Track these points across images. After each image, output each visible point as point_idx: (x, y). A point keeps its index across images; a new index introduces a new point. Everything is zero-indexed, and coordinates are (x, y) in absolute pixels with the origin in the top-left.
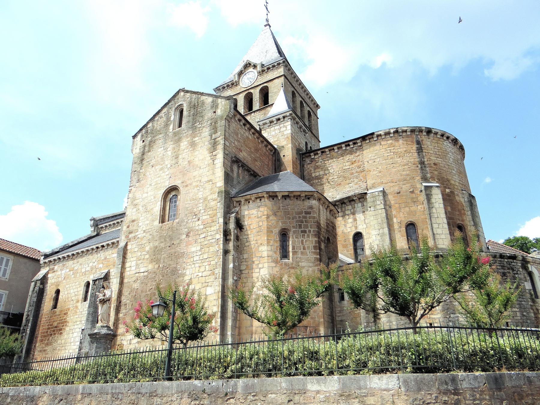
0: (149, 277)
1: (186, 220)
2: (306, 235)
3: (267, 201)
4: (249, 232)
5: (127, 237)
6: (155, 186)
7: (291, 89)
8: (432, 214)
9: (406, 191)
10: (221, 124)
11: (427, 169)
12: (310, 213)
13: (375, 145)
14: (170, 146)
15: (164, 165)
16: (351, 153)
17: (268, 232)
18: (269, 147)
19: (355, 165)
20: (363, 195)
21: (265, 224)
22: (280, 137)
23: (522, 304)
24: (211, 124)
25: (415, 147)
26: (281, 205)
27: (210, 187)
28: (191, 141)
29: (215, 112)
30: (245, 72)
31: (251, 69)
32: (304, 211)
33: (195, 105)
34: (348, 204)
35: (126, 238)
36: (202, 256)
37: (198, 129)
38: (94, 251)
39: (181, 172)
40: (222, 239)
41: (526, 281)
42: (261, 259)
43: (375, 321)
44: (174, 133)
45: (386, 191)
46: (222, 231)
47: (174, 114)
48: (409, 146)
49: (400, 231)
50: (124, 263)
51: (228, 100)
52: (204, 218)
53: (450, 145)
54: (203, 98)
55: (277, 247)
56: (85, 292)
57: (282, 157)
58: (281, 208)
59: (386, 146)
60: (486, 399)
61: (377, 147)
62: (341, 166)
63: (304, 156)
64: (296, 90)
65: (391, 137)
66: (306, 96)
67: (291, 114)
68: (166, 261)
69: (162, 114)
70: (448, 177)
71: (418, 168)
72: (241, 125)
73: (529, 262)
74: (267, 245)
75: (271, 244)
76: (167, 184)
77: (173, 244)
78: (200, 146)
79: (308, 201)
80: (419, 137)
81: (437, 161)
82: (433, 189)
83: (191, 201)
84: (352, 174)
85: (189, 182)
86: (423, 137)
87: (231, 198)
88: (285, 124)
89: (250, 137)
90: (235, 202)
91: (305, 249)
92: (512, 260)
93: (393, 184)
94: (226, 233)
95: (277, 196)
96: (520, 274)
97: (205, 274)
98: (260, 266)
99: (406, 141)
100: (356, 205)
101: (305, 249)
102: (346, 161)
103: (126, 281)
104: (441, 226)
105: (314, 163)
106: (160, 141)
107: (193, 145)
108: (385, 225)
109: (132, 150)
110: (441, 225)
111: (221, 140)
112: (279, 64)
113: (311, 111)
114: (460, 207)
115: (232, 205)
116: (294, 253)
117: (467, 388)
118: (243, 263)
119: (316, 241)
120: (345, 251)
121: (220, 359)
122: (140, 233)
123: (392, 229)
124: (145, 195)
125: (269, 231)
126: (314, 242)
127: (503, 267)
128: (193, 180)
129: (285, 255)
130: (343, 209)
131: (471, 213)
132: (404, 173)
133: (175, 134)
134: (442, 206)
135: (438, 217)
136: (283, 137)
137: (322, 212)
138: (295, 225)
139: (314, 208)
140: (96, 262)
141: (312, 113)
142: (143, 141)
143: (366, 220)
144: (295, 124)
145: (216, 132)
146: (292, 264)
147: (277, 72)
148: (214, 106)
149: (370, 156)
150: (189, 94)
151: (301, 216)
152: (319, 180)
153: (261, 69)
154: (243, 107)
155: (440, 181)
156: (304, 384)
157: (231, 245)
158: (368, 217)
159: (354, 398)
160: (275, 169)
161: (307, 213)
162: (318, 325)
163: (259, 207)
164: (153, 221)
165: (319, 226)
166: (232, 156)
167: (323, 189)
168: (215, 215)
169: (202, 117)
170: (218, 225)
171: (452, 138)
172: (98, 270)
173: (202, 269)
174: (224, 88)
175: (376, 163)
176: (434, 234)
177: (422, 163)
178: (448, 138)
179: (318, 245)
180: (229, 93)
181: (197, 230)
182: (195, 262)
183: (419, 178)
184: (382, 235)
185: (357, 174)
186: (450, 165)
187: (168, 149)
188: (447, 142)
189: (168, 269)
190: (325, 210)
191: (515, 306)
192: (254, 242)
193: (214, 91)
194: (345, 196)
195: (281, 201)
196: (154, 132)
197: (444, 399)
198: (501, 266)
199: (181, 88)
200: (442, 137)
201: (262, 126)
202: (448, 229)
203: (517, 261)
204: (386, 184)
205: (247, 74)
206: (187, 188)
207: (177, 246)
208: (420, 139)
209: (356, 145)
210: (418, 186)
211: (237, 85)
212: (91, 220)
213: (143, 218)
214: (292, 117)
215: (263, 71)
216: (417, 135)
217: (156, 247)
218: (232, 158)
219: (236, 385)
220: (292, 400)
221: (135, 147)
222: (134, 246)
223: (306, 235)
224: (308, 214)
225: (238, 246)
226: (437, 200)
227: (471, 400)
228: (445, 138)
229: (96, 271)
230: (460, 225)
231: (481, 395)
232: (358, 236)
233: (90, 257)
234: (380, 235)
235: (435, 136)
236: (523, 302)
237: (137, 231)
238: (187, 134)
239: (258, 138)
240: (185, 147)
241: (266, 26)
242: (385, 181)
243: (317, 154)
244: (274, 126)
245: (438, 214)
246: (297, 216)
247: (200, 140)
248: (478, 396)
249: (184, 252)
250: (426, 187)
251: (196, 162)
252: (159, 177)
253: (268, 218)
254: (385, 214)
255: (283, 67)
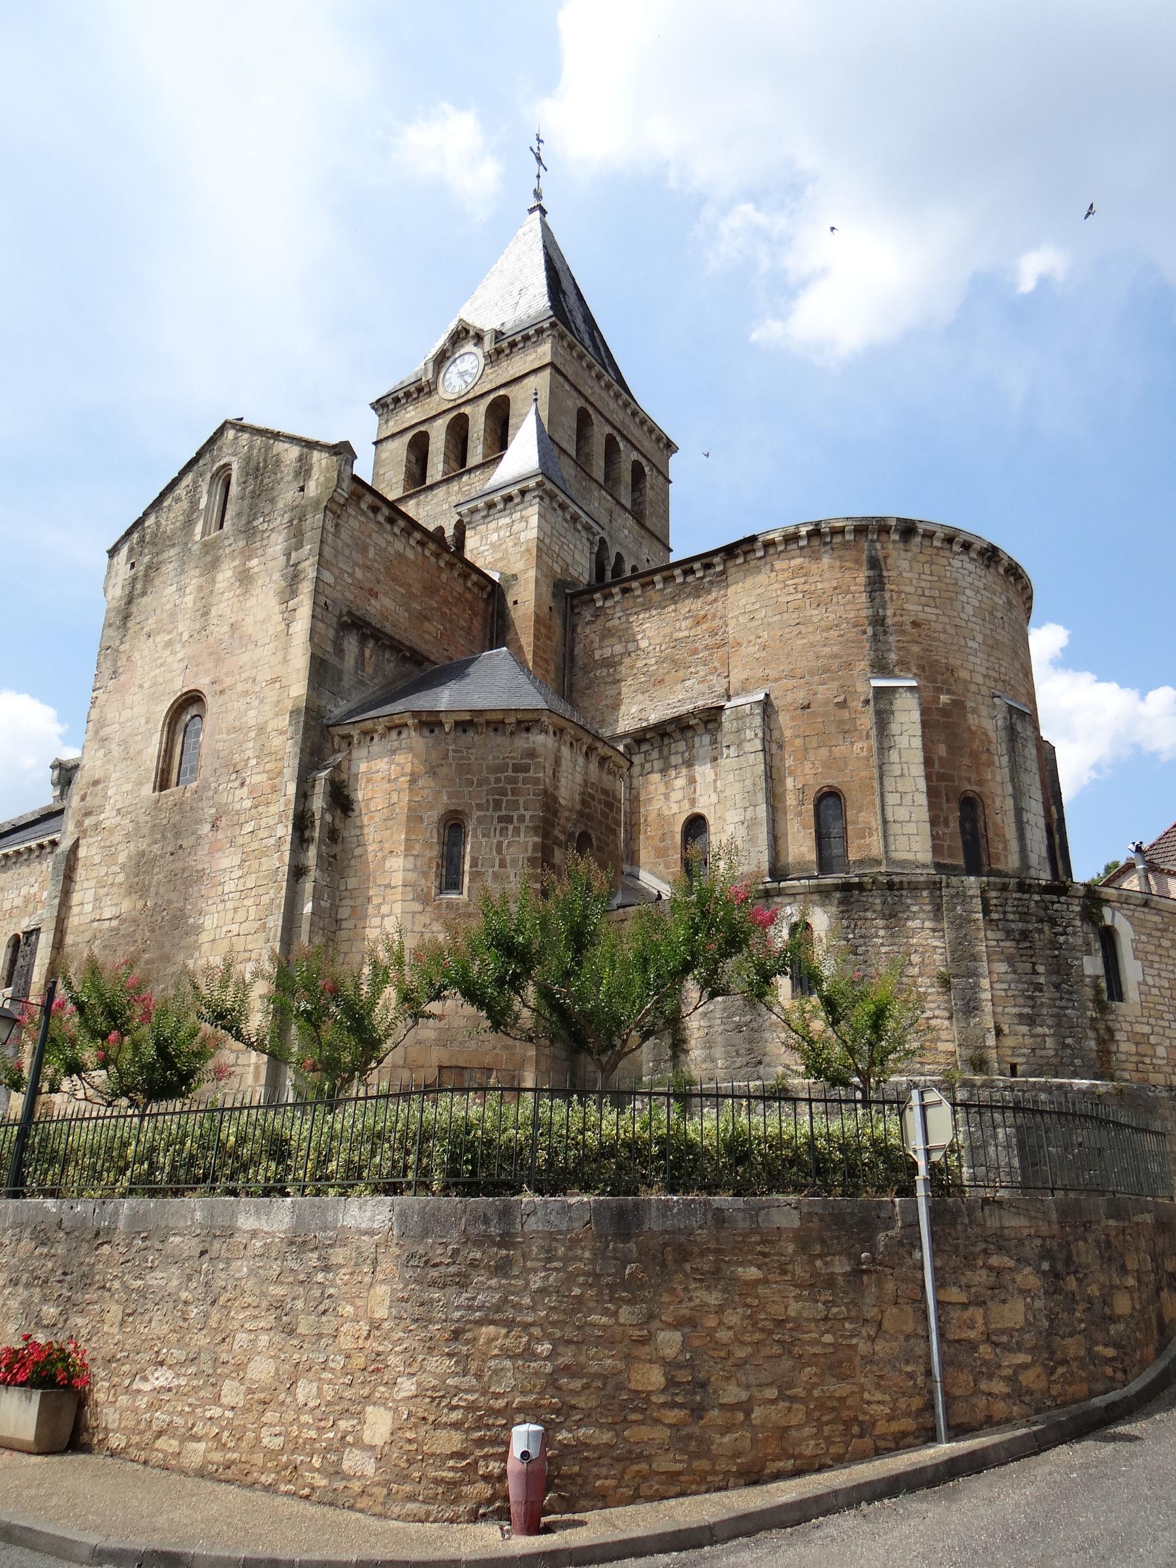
0: (122, 932)
1: (213, 785)
2: (511, 827)
3: (413, 738)
4: (365, 820)
5: (79, 824)
6: (152, 690)
7: (573, 403)
8: (885, 767)
9: (827, 702)
10: (315, 520)
11: (891, 639)
12: (526, 769)
13: (758, 570)
14: (193, 580)
15: (175, 633)
16: (697, 592)
17: (409, 819)
18: (474, 577)
19: (705, 626)
20: (713, 711)
21: (406, 798)
22: (511, 550)
23: (1065, 1015)
24: (291, 521)
25: (863, 575)
26: (452, 747)
27: (275, 699)
28: (241, 569)
29: (302, 489)
30: (453, 353)
31: (469, 347)
32: (511, 762)
33: (257, 469)
34: (677, 735)
35: (76, 827)
36: (242, 880)
37: (259, 537)
38: (33, 856)
39: (210, 654)
40: (289, 838)
41: (1089, 953)
42: (388, 890)
43: (675, 1058)
44: (205, 545)
45: (775, 703)
46: (291, 818)
47: (209, 492)
48: (848, 574)
49: (800, 814)
50: (66, 894)
51: (336, 454)
52: (256, 779)
53: (971, 567)
54: (280, 447)
55: (430, 859)
56: (8, 962)
57: (510, 604)
58: (451, 754)
59: (786, 575)
60: (581, 1260)
61: (762, 578)
62: (668, 630)
63: (575, 602)
64: (592, 405)
65: (802, 548)
66: (628, 420)
67: (539, 485)
68: (162, 890)
69: (180, 491)
70: (951, 660)
71: (865, 637)
72: (379, 523)
73: (1108, 901)
74: (406, 856)
75: (415, 853)
76: (179, 687)
77: (181, 847)
78: (260, 582)
79: (525, 735)
80: (878, 545)
81: (922, 616)
82: (898, 696)
83: (228, 733)
84: (695, 652)
85: (228, 682)
86: (892, 548)
87: (328, 726)
88: (524, 513)
89: (410, 554)
90: (336, 739)
91: (505, 867)
92: (1055, 898)
93: (794, 682)
94: (302, 822)
95: (440, 724)
96: (1075, 933)
97: (245, 928)
98: (385, 909)
99: (841, 558)
100: (697, 739)
101: (505, 867)
102: (681, 617)
103: (69, 939)
104: (908, 799)
105: (600, 621)
106: (171, 567)
107: (245, 578)
108: (761, 797)
109: (105, 590)
110: (909, 797)
111: (309, 570)
112: (540, 332)
113: (644, 462)
114: (976, 745)
115: (330, 745)
116: (475, 876)
117: (538, 1232)
118: (344, 902)
119: (535, 844)
120: (661, 867)
121: (110, 1149)
122: (108, 817)
123: (780, 806)
124: (127, 713)
125: (414, 817)
126: (530, 848)
127: (1024, 916)
128: (237, 677)
129: (450, 880)
130: (666, 750)
131: (1010, 761)
132: (827, 650)
133: (207, 547)
134: (917, 742)
135: (902, 775)
136: (518, 548)
137: (566, 764)
138: (484, 801)
139: (540, 756)
140: (36, 885)
141: (647, 469)
142: (133, 565)
143: (718, 783)
144: (555, 510)
145: (299, 545)
146: (467, 905)
147: (534, 355)
148: (303, 470)
149: (743, 602)
150: (246, 436)
151: (502, 776)
152: (611, 671)
153: (493, 346)
154: (441, 457)
155: (924, 671)
156: (234, 1216)
157: (311, 855)
158: (723, 775)
159: (312, 1250)
160: (491, 640)
161: (518, 768)
162: (521, 1065)
163: (393, 752)
164: (140, 784)
165: (550, 802)
166: (341, 613)
167: (619, 693)
168: (280, 773)
169: (272, 501)
170: (283, 800)
171: (978, 545)
172: (40, 905)
173: (241, 916)
174: (397, 400)
175: (755, 623)
176: (885, 822)
177: (878, 622)
178: (967, 546)
179: (540, 854)
180: (411, 415)
181: (238, 813)
182: (226, 897)
183: (863, 665)
184: (750, 824)
185: (706, 653)
186: (963, 624)
187: (188, 590)
188: (965, 558)
189: (165, 913)
190: (581, 760)
191: (1044, 1020)
192: (375, 847)
193: (373, 408)
194: (669, 714)
195: (451, 737)
196: (159, 542)
197: (471, 1255)
198: (1019, 913)
199: (231, 417)
200: (947, 546)
201: (467, 516)
202: (926, 808)
203: (1070, 900)
204: (776, 680)
205: (458, 361)
206: (223, 697)
207: (190, 854)
208: (881, 554)
209: (712, 571)
210: (861, 687)
211: (430, 392)
212: (53, 767)
213: (117, 775)
214: (545, 491)
215: (499, 352)
216: (873, 541)
217: (143, 854)
218: (341, 615)
219: (116, 1212)
220: (206, 1252)
221: (112, 582)
222: (94, 850)
223: (511, 827)
224: (522, 771)
225: (334, 857)
226: (905, 727)
227: (540, 1260)
228: (957, 548)
229: (35, 908)
230: (971, 794)
231: (570, 1249)
232: (696, 826)
233: (24, 870)
234: (746, 825)
235: (927, 542)
236: (1069, 1011)
237: (102, 808)
238: (233, 547)
239: (437, 556)
240: (226, 584)
241: (531, 211)
242: (773, 673)
243: (611, 595)
244: (497, 516)
245: (905, 766)
246: (492, 777)
247: (262, 566)
248: (561, 1251)
249: (204, 870)
250: (879, 691)
251: (249, 627)
252: (162, 665)
253: (413, 782)
254: (762, 767)
255: (550, 340)
